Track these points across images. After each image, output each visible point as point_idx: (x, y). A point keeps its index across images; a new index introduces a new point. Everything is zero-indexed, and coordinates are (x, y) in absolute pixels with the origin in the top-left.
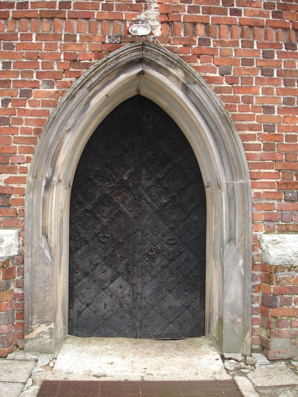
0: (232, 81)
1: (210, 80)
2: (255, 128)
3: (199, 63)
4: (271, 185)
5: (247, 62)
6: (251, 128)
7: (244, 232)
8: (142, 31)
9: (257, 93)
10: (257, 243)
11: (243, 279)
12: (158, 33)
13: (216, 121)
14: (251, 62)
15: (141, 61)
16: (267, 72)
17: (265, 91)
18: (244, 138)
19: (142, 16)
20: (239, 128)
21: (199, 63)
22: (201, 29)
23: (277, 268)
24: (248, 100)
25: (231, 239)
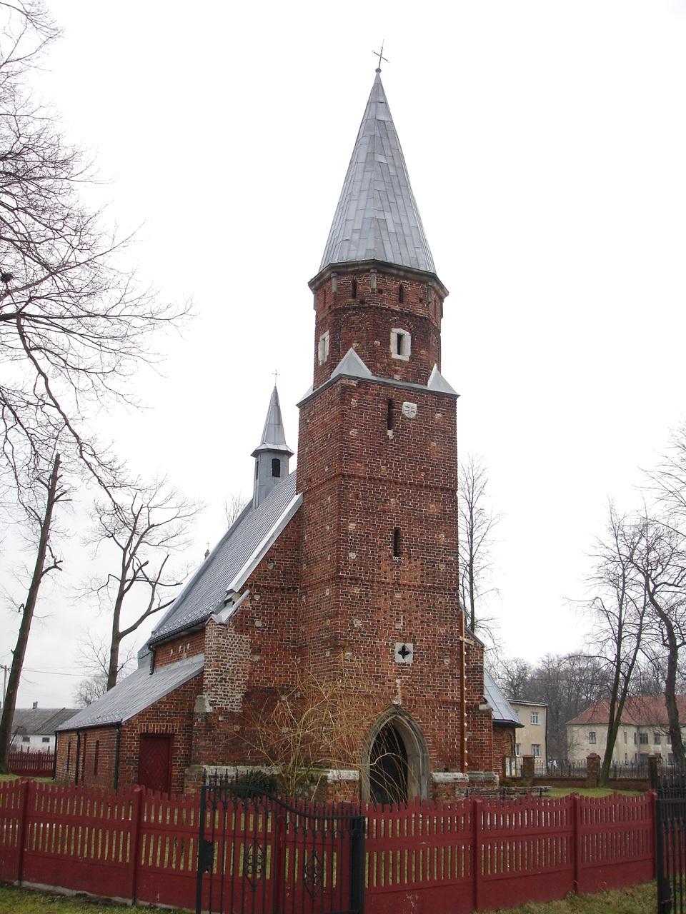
0: (423, 720)
1: (416, 719)
2: (318, 570)
3: (413, 714)
4: (435, 756)
5: (428, 713)
6: (429, 736)
7: (427, 771)
8: (396, 703)
9: (145, 738)
10: (431, 775)
11: (427, 788)
12: (400, 703)
13: (467, 584)
14: (428, 713)
15: (395, 713)
16: (434, 717)
17: (433, 723)
18: (427, 739)
19: (396, 697)
20: (426, 736)
21: (413, 714)
22: (414, 702)
23: (438, 784)
24: (427, 726)
25: (423, 774)
